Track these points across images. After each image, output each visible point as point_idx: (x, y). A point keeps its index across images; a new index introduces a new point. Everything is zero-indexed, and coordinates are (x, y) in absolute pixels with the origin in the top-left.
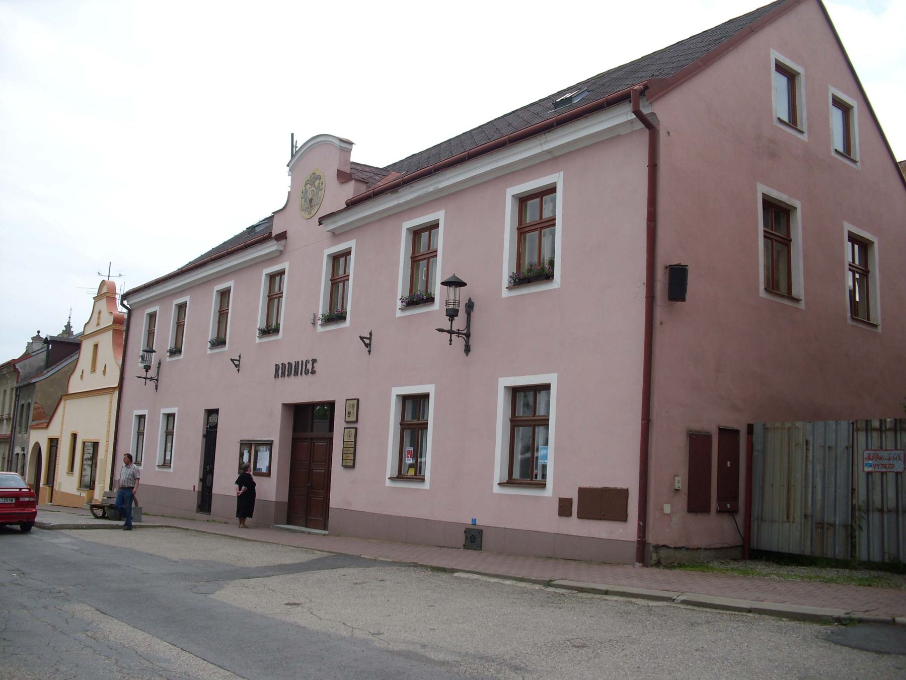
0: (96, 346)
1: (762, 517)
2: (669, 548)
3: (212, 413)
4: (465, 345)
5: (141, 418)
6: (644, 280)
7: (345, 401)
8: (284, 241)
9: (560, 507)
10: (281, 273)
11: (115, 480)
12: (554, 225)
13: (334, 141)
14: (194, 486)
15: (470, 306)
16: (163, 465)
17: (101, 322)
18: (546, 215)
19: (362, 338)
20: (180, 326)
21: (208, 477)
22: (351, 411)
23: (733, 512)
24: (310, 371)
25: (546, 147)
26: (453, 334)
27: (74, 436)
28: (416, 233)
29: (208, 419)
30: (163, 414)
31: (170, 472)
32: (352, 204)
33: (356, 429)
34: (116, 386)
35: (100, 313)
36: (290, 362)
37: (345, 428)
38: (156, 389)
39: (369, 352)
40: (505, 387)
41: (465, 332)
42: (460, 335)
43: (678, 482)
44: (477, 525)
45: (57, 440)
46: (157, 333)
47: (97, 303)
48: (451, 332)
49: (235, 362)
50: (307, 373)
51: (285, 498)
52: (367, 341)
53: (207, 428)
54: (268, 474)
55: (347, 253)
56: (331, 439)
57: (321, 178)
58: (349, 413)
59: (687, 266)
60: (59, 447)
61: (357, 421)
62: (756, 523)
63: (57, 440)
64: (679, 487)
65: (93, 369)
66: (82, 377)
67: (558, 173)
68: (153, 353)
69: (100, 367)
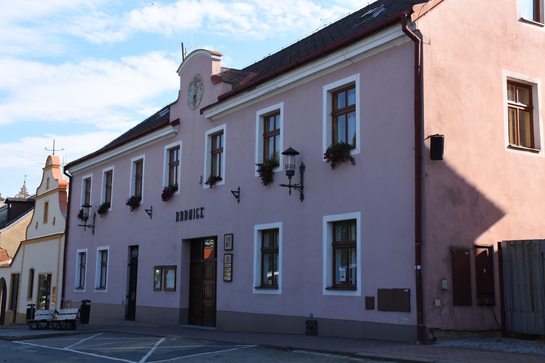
0: (47, 204)
1: (513, 309)
2: (441, 330)
3: (134, 248)
4: (300, 195)
5: (82, 254)
6: (414, 146)
7: (224, 236)
8: (178, 126)
9: (367, 303)
10: (177, 148)
11: (65, 302)
12: (355, 110)
13: (207, 54)
14: (123, 302)
15: (302, 168)
16: (100, 288)
17: (50, 186)
18: (350, 103)
19: (233, 192)
20: (108, 187)
21: (133, 294)
22: (228, 242)
23: (491, 305)
24: (200, 216)
25: (348, 56)
26: (292, 187)
27: (32, 271)
28: (266, 118)
29: (131, 253)
30: (79, 253)
31: (105, 293)
32: (222, 99)
33: (232, 255)
34: (63, 232)
35: (48, 179)
36: (186, 210)
37: (225, 254)
38: (93, 233)
39: (239, 201)
40: (327, 222)
41: (300, 185)
42: (296, 188)
43: (445, 284)
44: (314, 318)
45: (19, 275)
46: (92, 193)
47: (45, 172)
48: (290, 186)
49: (148, 211)
50: (198, 217)
51: (187, 306)
52: (236, 194)
53: (131, 259)
54: (175, 289)
55: (221, 133)
56: (216, 262)
57: (200, 81)
58: (227, 244)
59: (443, 135)
60: (20, 280)
61: (232, 249)
62: (509, 312)
63: (19, 275)
64: (445, 288)
65: (45, 220)
66: (37, 227)
67: (356, 75)
68: (90, 208)
69: (50, 219)
